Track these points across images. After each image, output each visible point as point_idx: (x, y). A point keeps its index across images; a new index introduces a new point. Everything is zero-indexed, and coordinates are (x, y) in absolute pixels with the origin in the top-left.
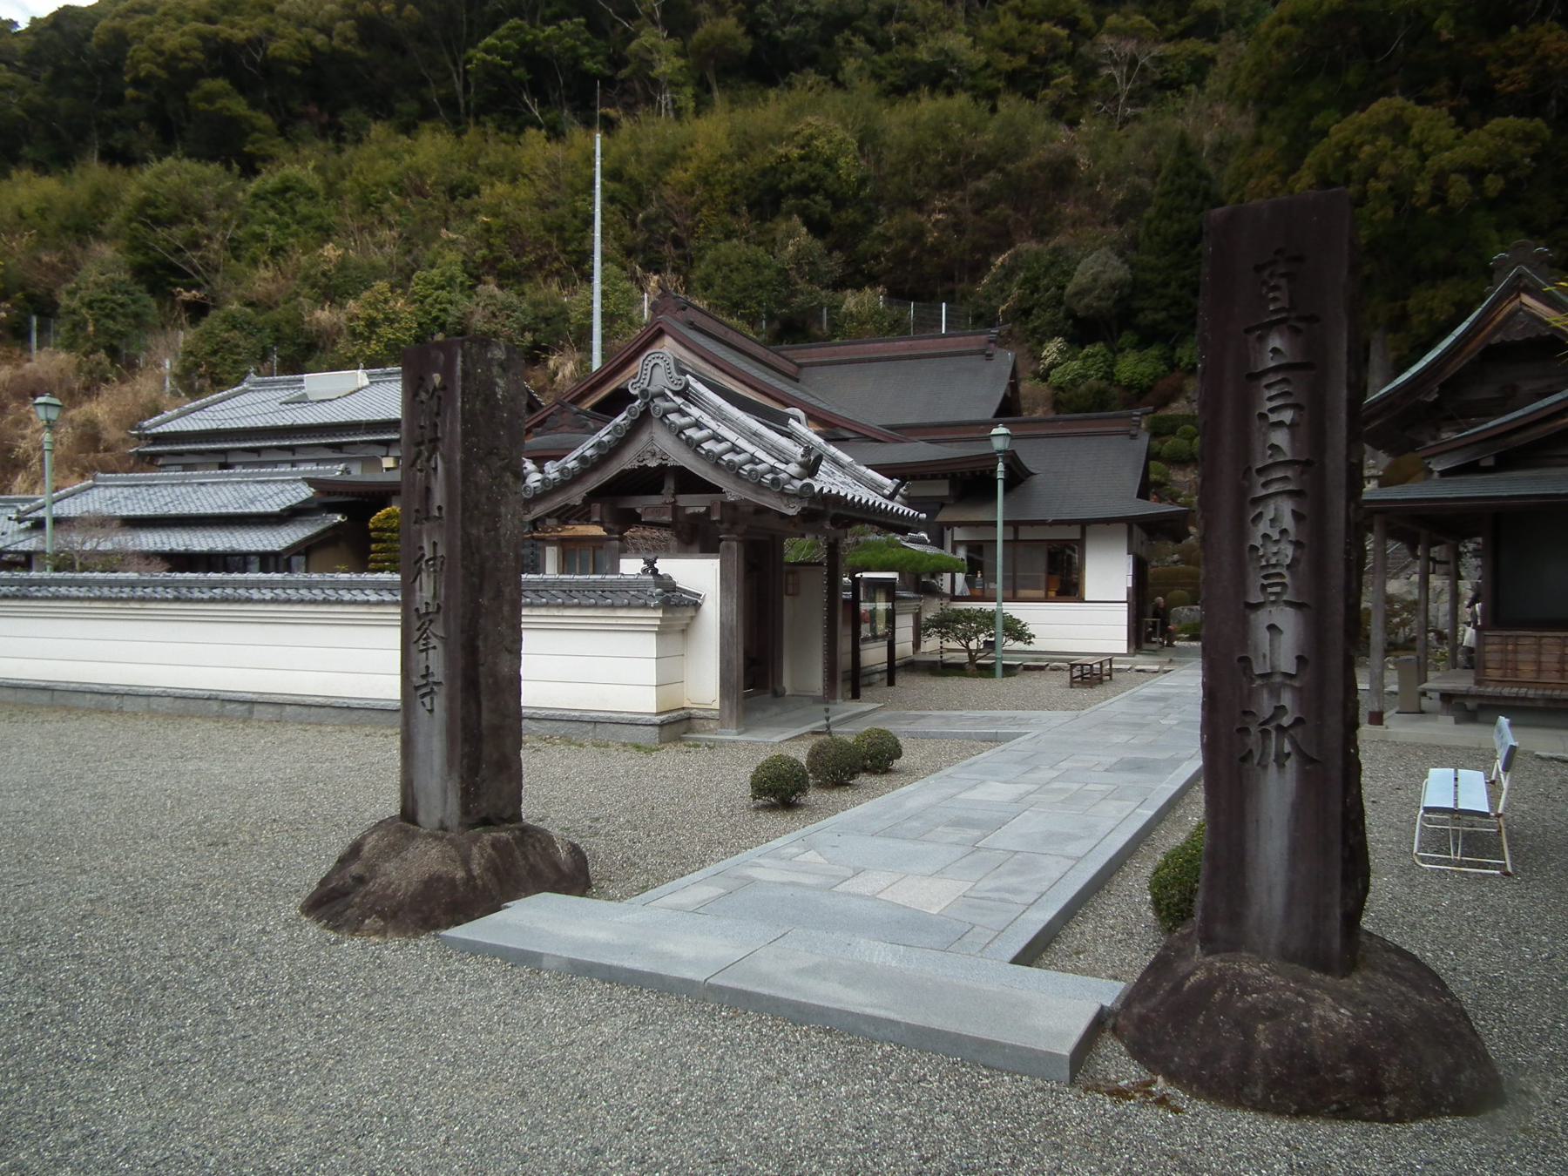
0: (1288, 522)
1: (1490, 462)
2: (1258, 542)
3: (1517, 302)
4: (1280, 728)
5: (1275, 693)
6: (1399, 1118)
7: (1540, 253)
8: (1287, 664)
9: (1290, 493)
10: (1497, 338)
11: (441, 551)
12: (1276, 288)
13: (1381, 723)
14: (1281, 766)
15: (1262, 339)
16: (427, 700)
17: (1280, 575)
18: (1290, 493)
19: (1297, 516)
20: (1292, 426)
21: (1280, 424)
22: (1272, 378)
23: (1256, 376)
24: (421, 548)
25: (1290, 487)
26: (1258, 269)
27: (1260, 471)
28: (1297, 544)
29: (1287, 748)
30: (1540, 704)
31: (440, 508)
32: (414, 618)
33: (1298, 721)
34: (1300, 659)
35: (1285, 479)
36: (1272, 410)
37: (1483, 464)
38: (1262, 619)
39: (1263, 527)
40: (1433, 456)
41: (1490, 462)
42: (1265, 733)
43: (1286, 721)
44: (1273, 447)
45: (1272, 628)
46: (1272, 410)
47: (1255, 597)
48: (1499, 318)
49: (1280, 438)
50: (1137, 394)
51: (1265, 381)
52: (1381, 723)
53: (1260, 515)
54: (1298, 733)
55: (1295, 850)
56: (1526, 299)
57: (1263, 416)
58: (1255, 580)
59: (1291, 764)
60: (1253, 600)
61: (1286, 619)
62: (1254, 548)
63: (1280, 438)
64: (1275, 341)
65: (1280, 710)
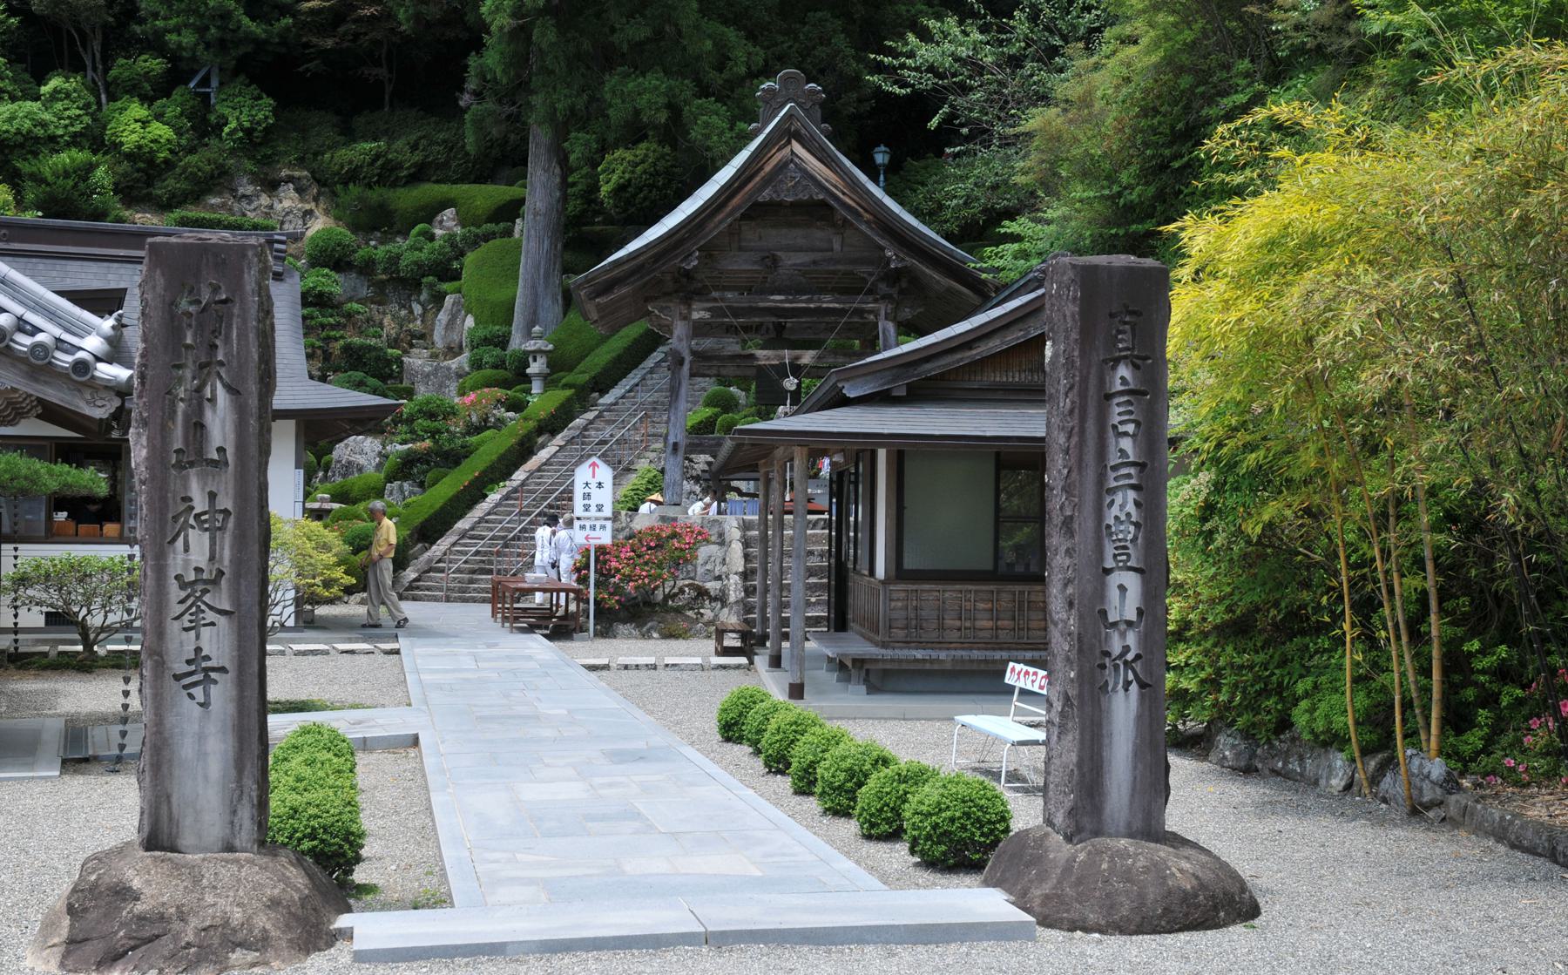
0: (1131, 508)
1: (903, 392)
2: (1112, 522)
3: (787, 151)
4: (1126, 663)
5: (1123, 635)
6: (1225, 925)
7: (812, 91)
8: (1131, 615)
9: (1133, 487)
10: (766, 195)
11: (225, 502)
12: (1124, 332)
13: (802, 697)
14: (1126, 690)
15: (1114, 368)
16: (198, 692)
17: (1125, 547)
18: (1133, 487)
19: (1137, 504)
20: (1134, 436)
21: (1126, 434)
22: (1122, 399)
23: (1109, 397)
24: (187, 499)
25: (1133, 481)
26: (1111, 315)
27: (1114, 468)
28: (1137, 525)
29: (1131, 676)
30: (948, 666)
31: (221, 450)
32: (173, 586)
33: (1138, 657)
34: (1140, 612)
35: (1129, 476)
36: (1121, 423)
37: (895, 393)
38: (1116, 579)
39: (1115, 511)
40: (847, 380)
41: (903, 392)
42: (1116, 667)
43: (1130, 657)
44: (1121, 450)
45: (1122, 588)
46: (1121, 423)
47: (1109, 564)
48: (768, 168)
49: (1126, 444)
50: (144, 179)
51: (1116, 400)
52: (802, 697)
53: (1113, 502)
54: (1138, 666)
55: (1137, 754)
56: (797, 147)
57: (1114, 427)
58: (1109, 551)
59: (1134, 687)
60: (1108, 566)
61: (1132, 581)
62: (1109, 527)
63: (1126, 444)
64: (1123, 371)
65: (1126, 649)
